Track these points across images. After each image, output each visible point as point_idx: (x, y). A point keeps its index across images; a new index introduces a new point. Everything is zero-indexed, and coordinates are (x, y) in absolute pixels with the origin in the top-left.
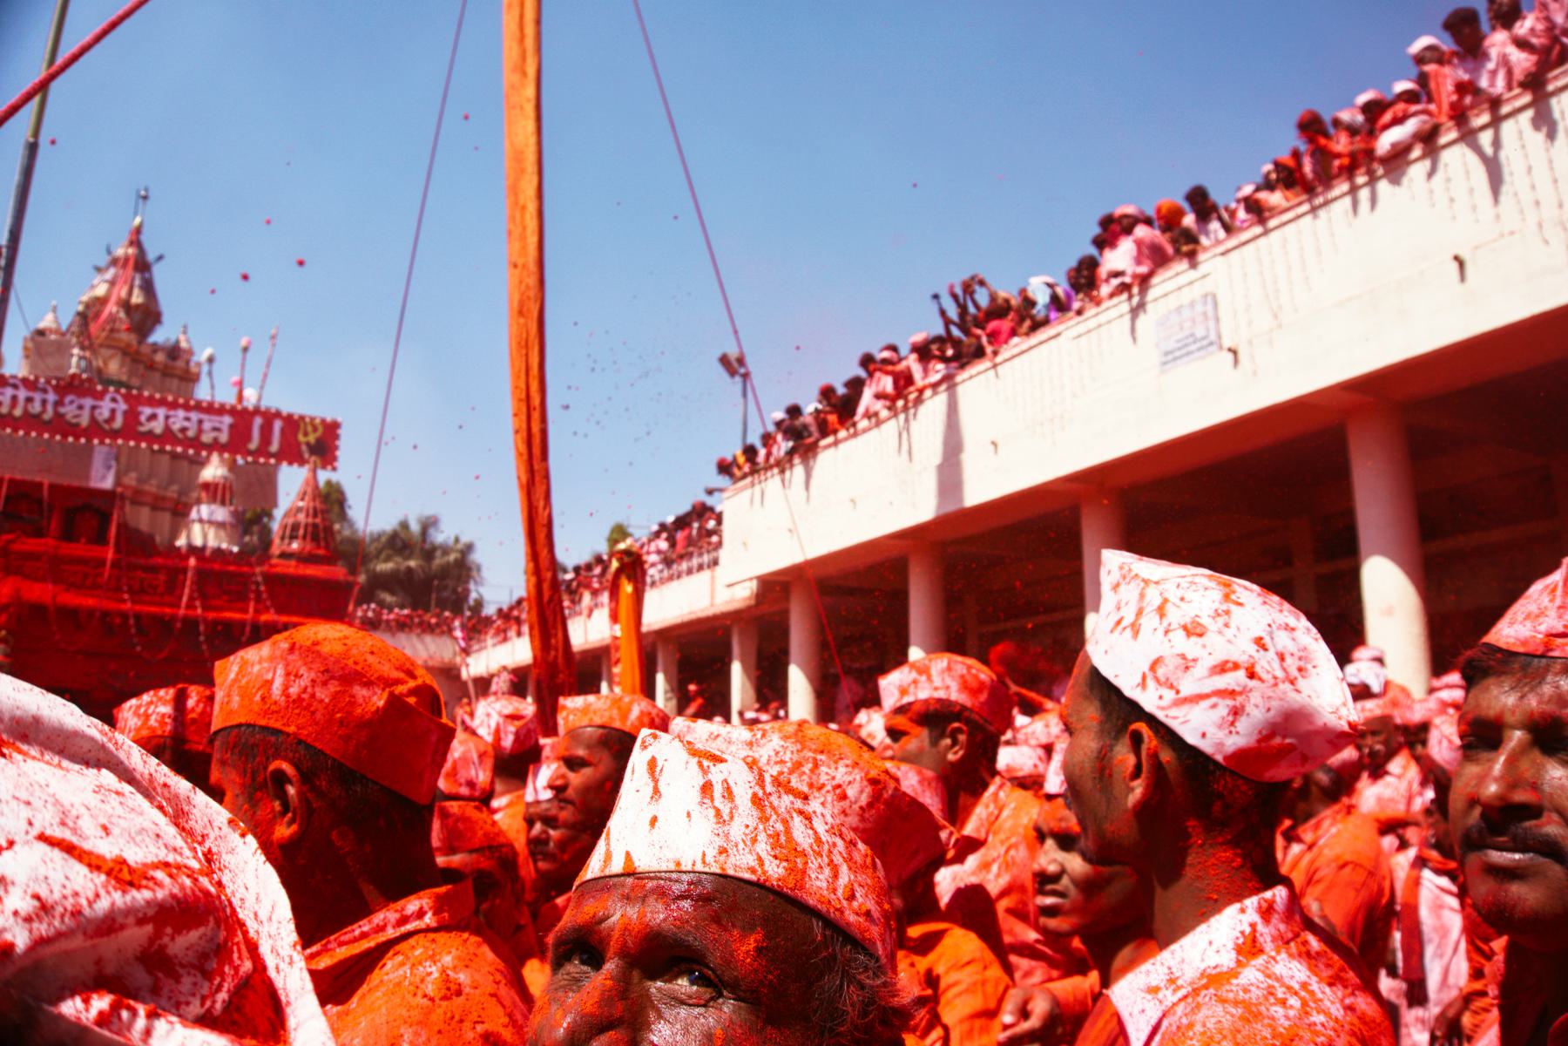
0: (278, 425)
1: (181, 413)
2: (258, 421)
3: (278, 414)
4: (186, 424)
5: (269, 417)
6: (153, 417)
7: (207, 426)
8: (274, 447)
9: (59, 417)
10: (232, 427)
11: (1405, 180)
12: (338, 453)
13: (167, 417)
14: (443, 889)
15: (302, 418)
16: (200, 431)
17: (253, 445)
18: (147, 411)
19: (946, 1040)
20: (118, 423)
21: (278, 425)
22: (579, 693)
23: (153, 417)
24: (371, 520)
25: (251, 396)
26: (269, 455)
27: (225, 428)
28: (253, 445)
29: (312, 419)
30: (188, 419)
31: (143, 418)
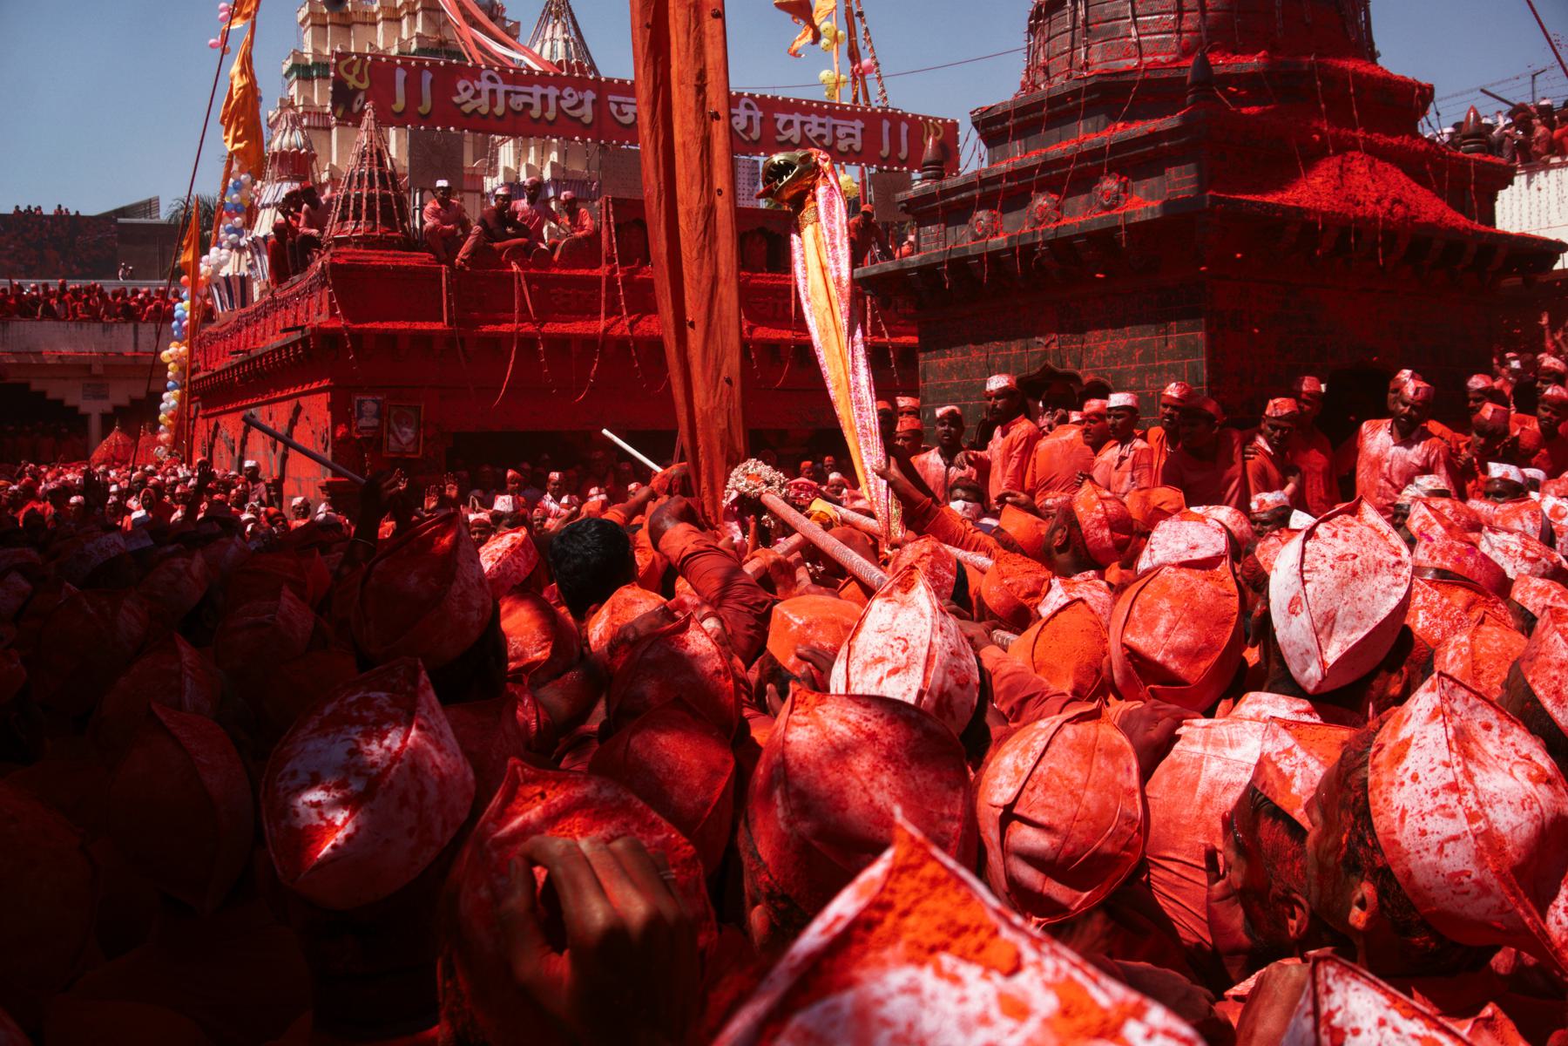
0: (904, 127)
1: (814, 119)
2: (886, 125)
3: (904, 116)
4: (822, 131)
5: (896, 118)
6: (789, 124)
7: (840, 132)
8: (903, 155)
9: (561, 87)
10: (863, 130)
11: (1424, 81)
12: (1410, 77)
13: (803, 124)
14: (1350, 65)
15: (926, 119)
16: (835, 138)
17: (885, 152)
18: (782, 118)
19: (1557, 615)
20: (756, 134)
21: (904, 127)
22: (741, 881)
23: (789, 124)
24: (297, 454)
25: (876, 103)
26: (901, 163)
27: (858, 133)
28: (885, 152)
29: (936, 119)
30: (821, 125)
31: (780, 126)
